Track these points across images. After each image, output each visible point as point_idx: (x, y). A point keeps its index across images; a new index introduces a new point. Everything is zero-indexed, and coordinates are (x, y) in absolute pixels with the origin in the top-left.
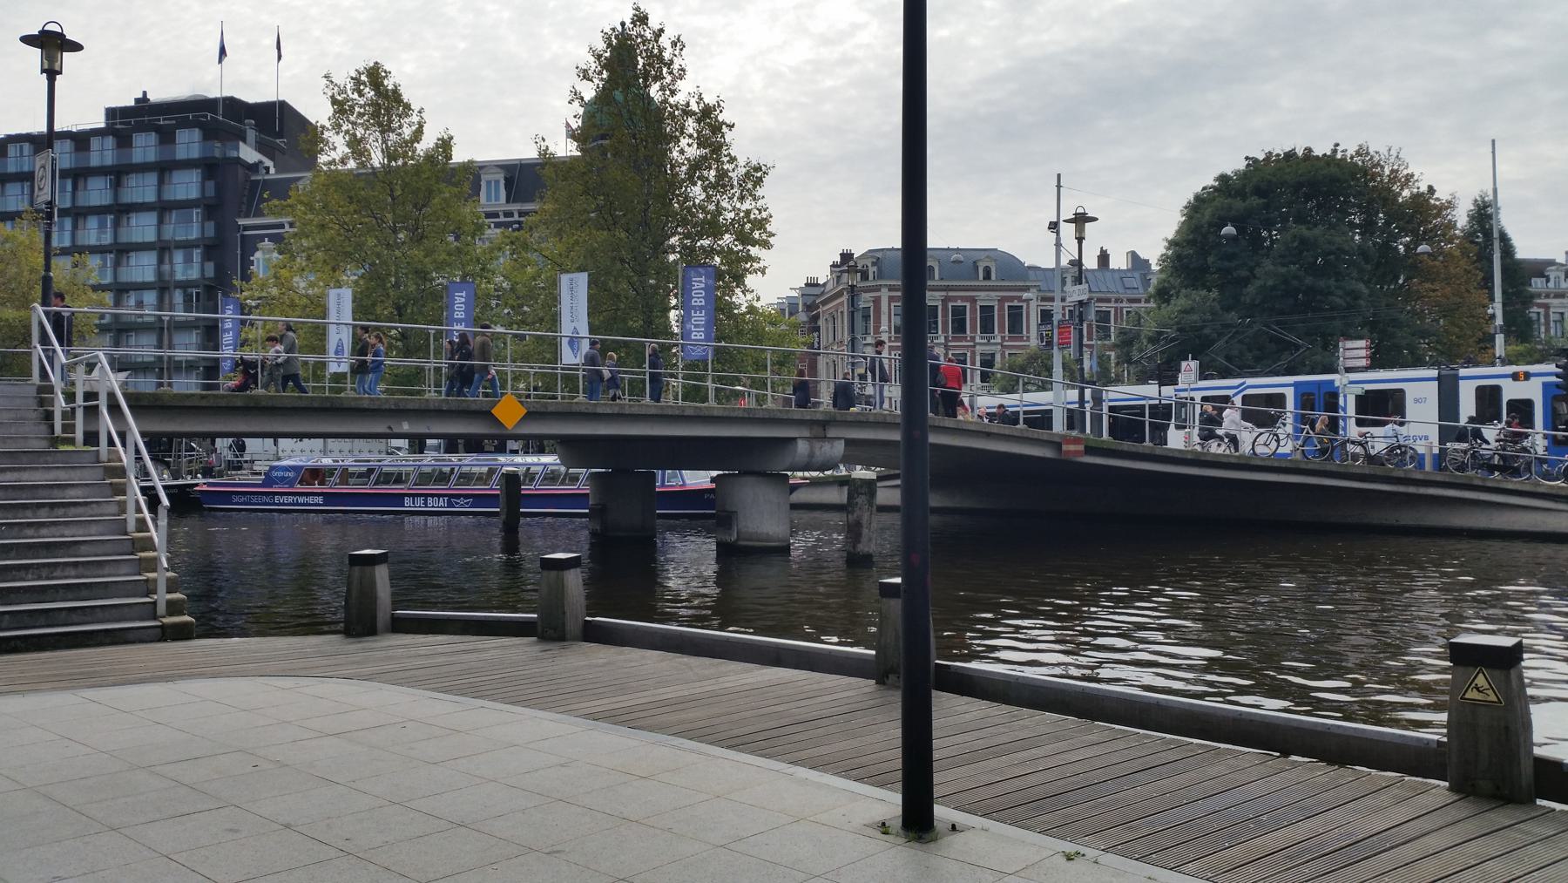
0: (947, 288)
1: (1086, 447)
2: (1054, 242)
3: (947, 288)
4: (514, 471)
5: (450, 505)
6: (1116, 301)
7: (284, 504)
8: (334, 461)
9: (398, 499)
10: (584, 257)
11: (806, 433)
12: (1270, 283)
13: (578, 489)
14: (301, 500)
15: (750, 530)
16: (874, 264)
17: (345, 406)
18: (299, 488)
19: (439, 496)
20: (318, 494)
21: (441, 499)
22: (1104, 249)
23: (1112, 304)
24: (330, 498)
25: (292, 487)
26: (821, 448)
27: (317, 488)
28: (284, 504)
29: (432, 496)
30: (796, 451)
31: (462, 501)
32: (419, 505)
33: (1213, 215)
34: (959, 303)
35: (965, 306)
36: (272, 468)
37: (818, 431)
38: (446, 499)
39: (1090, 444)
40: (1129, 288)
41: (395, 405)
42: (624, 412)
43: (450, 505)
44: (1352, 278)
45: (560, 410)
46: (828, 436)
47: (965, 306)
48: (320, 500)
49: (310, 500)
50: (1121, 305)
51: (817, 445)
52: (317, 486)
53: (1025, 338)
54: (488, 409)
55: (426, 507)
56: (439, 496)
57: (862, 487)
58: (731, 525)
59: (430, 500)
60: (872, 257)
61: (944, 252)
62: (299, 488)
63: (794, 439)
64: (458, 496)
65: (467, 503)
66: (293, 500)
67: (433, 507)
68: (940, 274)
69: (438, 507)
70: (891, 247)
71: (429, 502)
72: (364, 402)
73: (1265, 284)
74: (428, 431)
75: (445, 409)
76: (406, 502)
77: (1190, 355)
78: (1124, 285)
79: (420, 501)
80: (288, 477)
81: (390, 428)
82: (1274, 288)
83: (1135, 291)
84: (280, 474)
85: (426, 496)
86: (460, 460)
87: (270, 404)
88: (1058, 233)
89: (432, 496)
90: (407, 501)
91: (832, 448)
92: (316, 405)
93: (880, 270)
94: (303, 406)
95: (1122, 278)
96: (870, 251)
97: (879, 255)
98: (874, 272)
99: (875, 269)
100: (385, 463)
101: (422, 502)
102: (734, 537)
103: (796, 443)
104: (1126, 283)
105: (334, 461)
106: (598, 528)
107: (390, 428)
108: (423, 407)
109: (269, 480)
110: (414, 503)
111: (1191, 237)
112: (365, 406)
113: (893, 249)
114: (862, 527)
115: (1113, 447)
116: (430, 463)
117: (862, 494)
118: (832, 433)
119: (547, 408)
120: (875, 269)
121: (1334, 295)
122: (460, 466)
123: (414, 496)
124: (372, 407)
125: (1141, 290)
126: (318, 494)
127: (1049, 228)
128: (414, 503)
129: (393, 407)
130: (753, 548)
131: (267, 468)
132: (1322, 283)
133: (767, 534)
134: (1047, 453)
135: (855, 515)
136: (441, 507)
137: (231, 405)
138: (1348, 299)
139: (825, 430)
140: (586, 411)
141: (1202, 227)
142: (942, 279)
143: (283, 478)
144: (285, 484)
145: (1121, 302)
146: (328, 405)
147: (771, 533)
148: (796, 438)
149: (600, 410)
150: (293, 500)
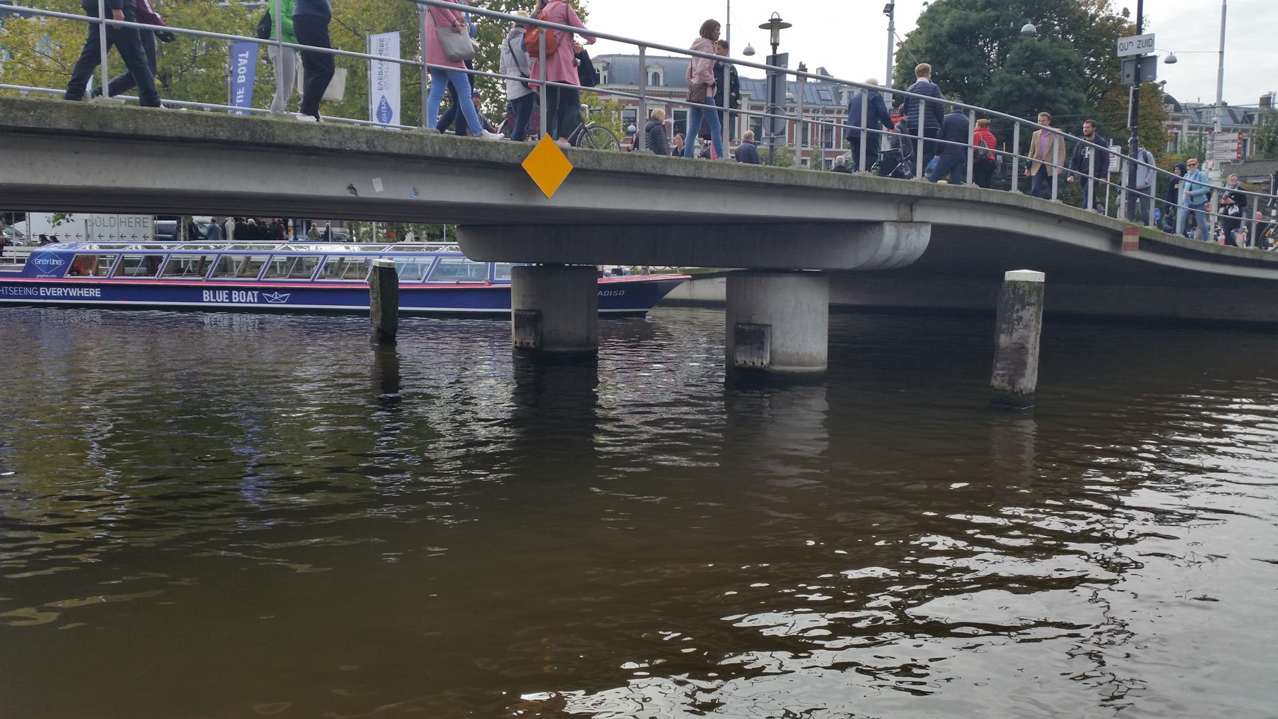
0: (671, 95)
1: (1141, 239)
2: (888, 27)
3: (671, 95)
4: (390, 264)
5: (261, 300)
6: (814, 111)
7: (51, 297)
8: (101, 247)
9: (196, 292)
10: (395, 16)
11: (893, 216)
12: (1006, 89)
13: (424, 283)
14: (73, 292)
15: (790, 350)
16: (605, 69)
17: (279, 140)
18: (68, 278)
19: (246, 290)
20: (94, 286)
21: (250, 293)
22: (803, 64)
23: (835, 115)
24: (108, 290)
25: (61, 277)
26: (908, 236)
27: (91, 278)
28: (51, 297)
29: (239, 289)
30: (880, 241)
31: (276, 295)
32: (221, 300)
33: (953, 25)
34: (681, 109)
35: (686, 112)
36: (34, 255)
37: (905, 210)
38: (256, 293)
39: (1146, 236)
40: (824, 100)
41: (367, 142)
42: (701, 175)
43: (261, 300)
44: (1071, 88)
45: (619, 168)
46: (915, 220)
47: (686, 112)
48: (96, 293)
49: (84, 292)
50: (818, 115)
51: (905, 231)
52: (91, 276)
53: (736, 143)
54: (513, 159)
55: (231, 302)
56: (246, 290)
57: (1030, 294)
58: (762, 343)
59: (235, 294)
60: (603, 61)
61: (667, 60)
62: (68, 278)
63: (879, 224)
64: (271, 290)
65: (283, 299)
66: (63, 293)
67: (239, 302)
68: (664, 81)
69: (246, 302)
70: (617, 53)
71: (234, 296)
72: (313, 133)
73: (1001, 90)
74: (415, 198)
75: (450, 156)
76: (204, 295)
77: (1111, 140)
78: (820, 98)
79: (223, 295)
80: (56, 266)
81: (351, 188)
82: (1010, 93)
83: (829, 103)
84: (45, 262)
85: (231, 289)
86: (217, 247)
87: (131, 127)
88: (891, 18)
89: (239, 289)
90: (206, 295)
91: (918, 236)
92: (223, 134)
93: (610, 74)
94: (198, 135)
95: (818, 91)
96: (600, 56)
97: (609, 60)
98: (605, 77)
99: (606, 73)
100: (127, 250)
101: (225, 296)
102: (766, 361)
103: (882, 230)
104: (821, 95)
105: (101, 247)
106: (532, 341)
107: (351, 188)
108: (415, 149)
109: (30, 269)
110: (215, 298)
111: (930, 45)
112: (316, 142)
113: (634, 56)
114: (1027, 353)
115: (1158, 239)
116: (180, 251)
117: (1030, 304)
118: (919, 215)
119: (599, 163)
120: (606, 73)
121: (1060, 103)
122: (169, 254)
123: (214, 289)
124: (327, 144)
125: (834, 102)
126: (94, 286)
127: (885, 11)
128: (215, 298)
129: (364, 147)
130: (793, 374)
131: (28, 254)
132: (1051, 91)
133: (811, 355)
134: (1098, 244)
135: (1016, 335)
136: (250, 302)
137: (43, 125)
138: (1071, 106)
139: (912, 211)
140: (653, 171)
141: (941, 36)
142: (666, 85)
143: (49, 267)
144: (51, 274)
145: (818, 112)
146: (246, 136)
147: (814, 354)
148: (884, 221)
149: (670, 171)
150: (63, 293)
